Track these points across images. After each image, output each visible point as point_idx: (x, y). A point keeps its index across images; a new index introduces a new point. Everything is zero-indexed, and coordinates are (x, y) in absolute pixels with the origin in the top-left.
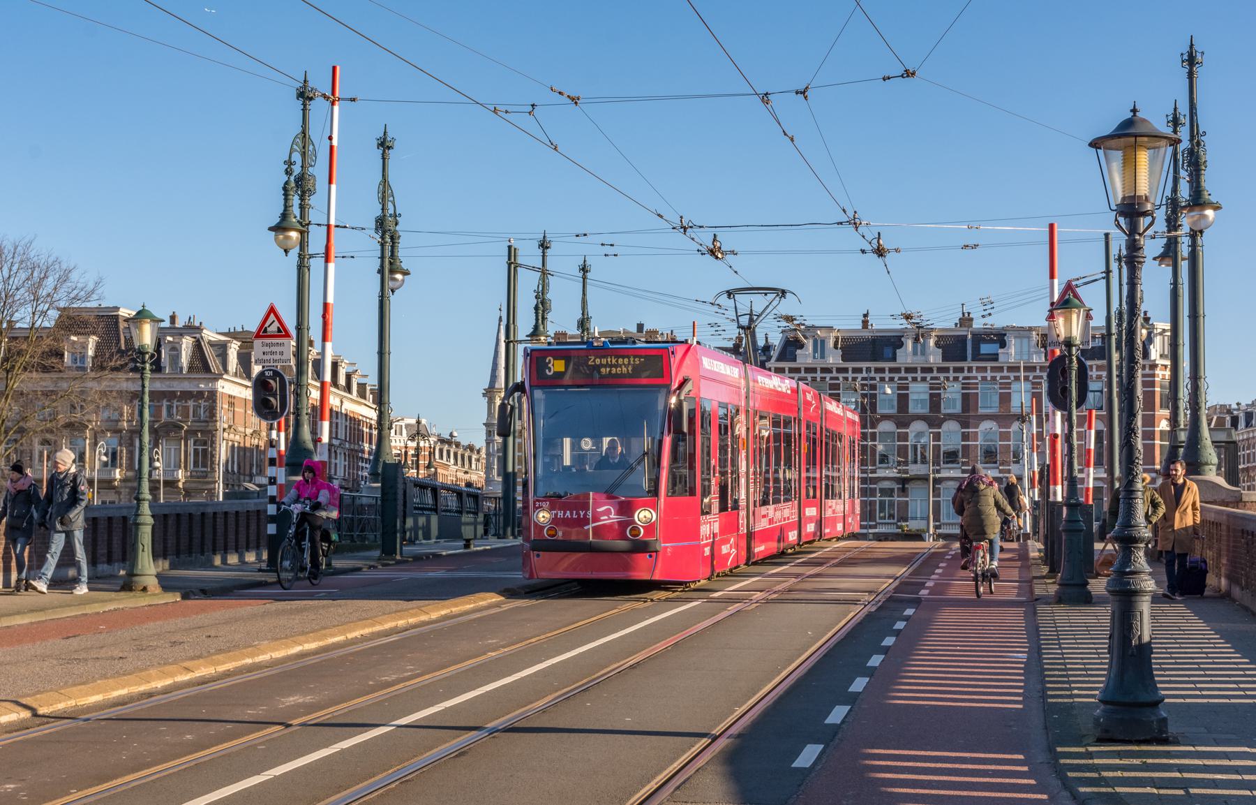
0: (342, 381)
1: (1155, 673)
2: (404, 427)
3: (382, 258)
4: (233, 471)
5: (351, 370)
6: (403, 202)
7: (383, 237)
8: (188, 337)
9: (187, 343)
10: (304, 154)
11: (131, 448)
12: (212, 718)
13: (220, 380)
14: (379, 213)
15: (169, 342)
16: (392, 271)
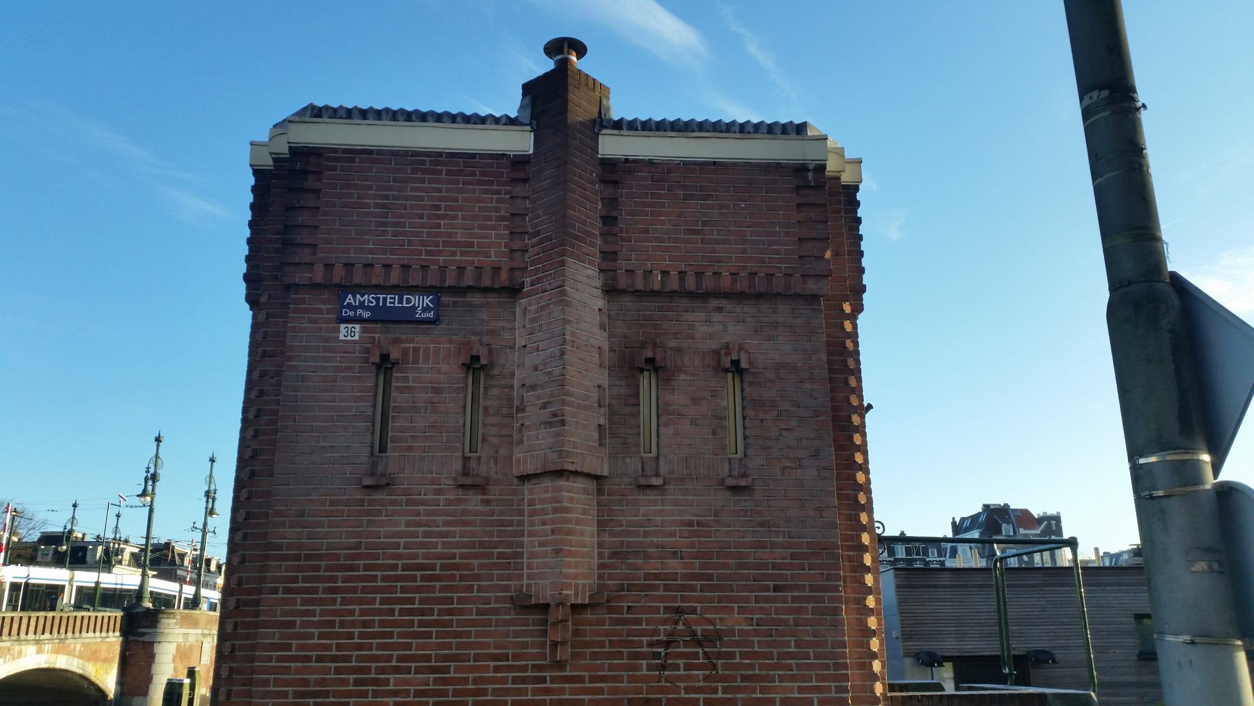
3: (206, 508)
14: (207, 489)
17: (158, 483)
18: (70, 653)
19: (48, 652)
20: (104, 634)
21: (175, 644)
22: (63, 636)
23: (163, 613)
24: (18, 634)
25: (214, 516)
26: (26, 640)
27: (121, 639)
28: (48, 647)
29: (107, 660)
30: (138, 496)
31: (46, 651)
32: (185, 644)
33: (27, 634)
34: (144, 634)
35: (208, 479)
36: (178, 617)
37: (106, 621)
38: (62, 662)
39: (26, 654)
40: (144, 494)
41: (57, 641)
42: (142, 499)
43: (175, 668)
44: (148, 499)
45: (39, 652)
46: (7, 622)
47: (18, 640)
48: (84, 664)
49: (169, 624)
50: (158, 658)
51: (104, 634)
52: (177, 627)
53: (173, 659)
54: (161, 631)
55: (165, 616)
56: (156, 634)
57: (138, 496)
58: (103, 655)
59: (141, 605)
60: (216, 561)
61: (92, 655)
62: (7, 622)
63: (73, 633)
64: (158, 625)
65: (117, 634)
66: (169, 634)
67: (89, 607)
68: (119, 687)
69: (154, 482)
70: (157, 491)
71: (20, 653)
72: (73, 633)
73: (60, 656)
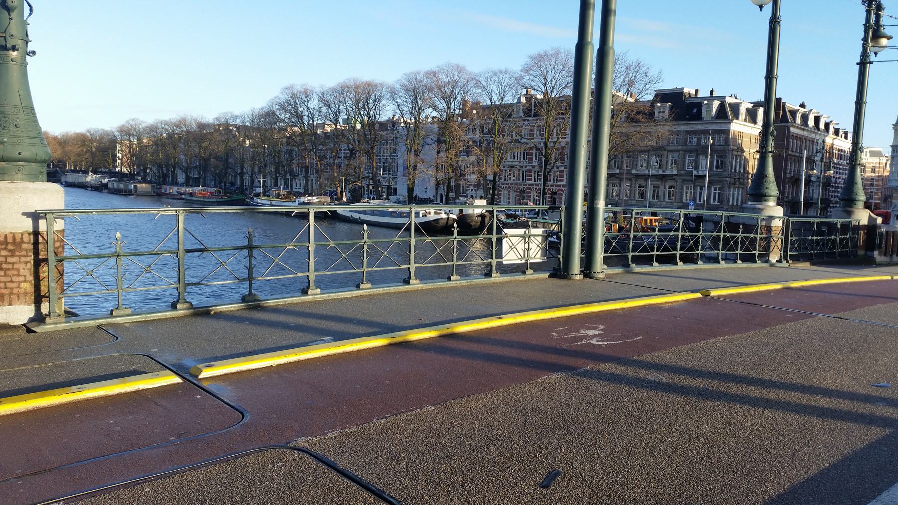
0: (822, 126)
1: (348, 152)
2: (868, 152)
4: (740, 171)
5: (828, 120)
8: (716, 101)
9: (716, 104)
11: (684, 159)
12: (674, 278)
13: (732, 123)
15: (706, 104)
25: (884, 42)
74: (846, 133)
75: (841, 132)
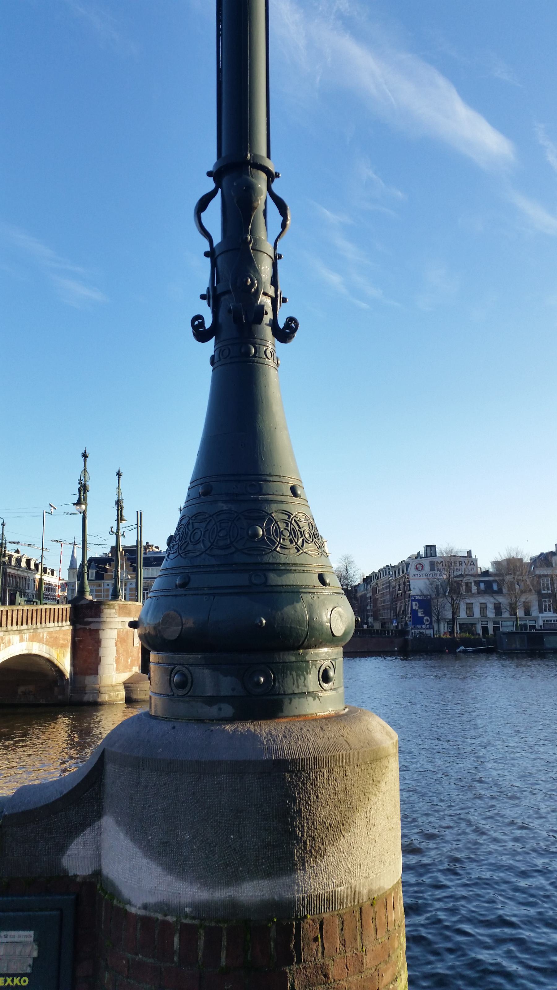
6: (124, 495)
7: (118, 507)
10: (85, 477)
14: (116, 499)
16: (122, 520)
17: (88, 494)
18: (40, 641)
19: (26, 641)
20: (60, 624)
21: (116, 630)
22: (34, 626)
23: (105, 604)
24: (7, 626)
25: (123, 522)
26: (12, 631)
27: (71, 627)
28: (26, 636)
29: (63, 646)
30: (74, 504)
31: (25, 639)
32: (123, 630)
33: (12, 626)
34: (89, 623)
35: (117, 490)
36: (117, 608)
37: (56, 611)
38: (37, 649)
39: (13, 643)
40: (79, 503)
41: (32, 631)
42: (78, 507)
43: (117, 651)
44: (83, 507)
45: (22, 640)
46: (4, 613)
47: (7, 631)
48: (50, 650)
49: (110, 614)
50: (104, 643)
51: (60, 624)
52: (117, 616)
53: (116, 643)
54: (105, 619)
55: (107, 607)
56: (100, 623)
57: (74, 504)
58: (61, 642)
59: (84, 598)
60: (34, 561)
61: (54, 642)
62: (4, 613)
63: (41, 623)
64: (102, 615)
65: (68, 623)
66: (111, 622)
67: (37, 600)
68: (72, 668)
69: (84, 493)
70: (88, 499)
71: (9, 641)
72: (41, 623)
73: (34, 643)
74: (52, 571)
75: (48, 571)
